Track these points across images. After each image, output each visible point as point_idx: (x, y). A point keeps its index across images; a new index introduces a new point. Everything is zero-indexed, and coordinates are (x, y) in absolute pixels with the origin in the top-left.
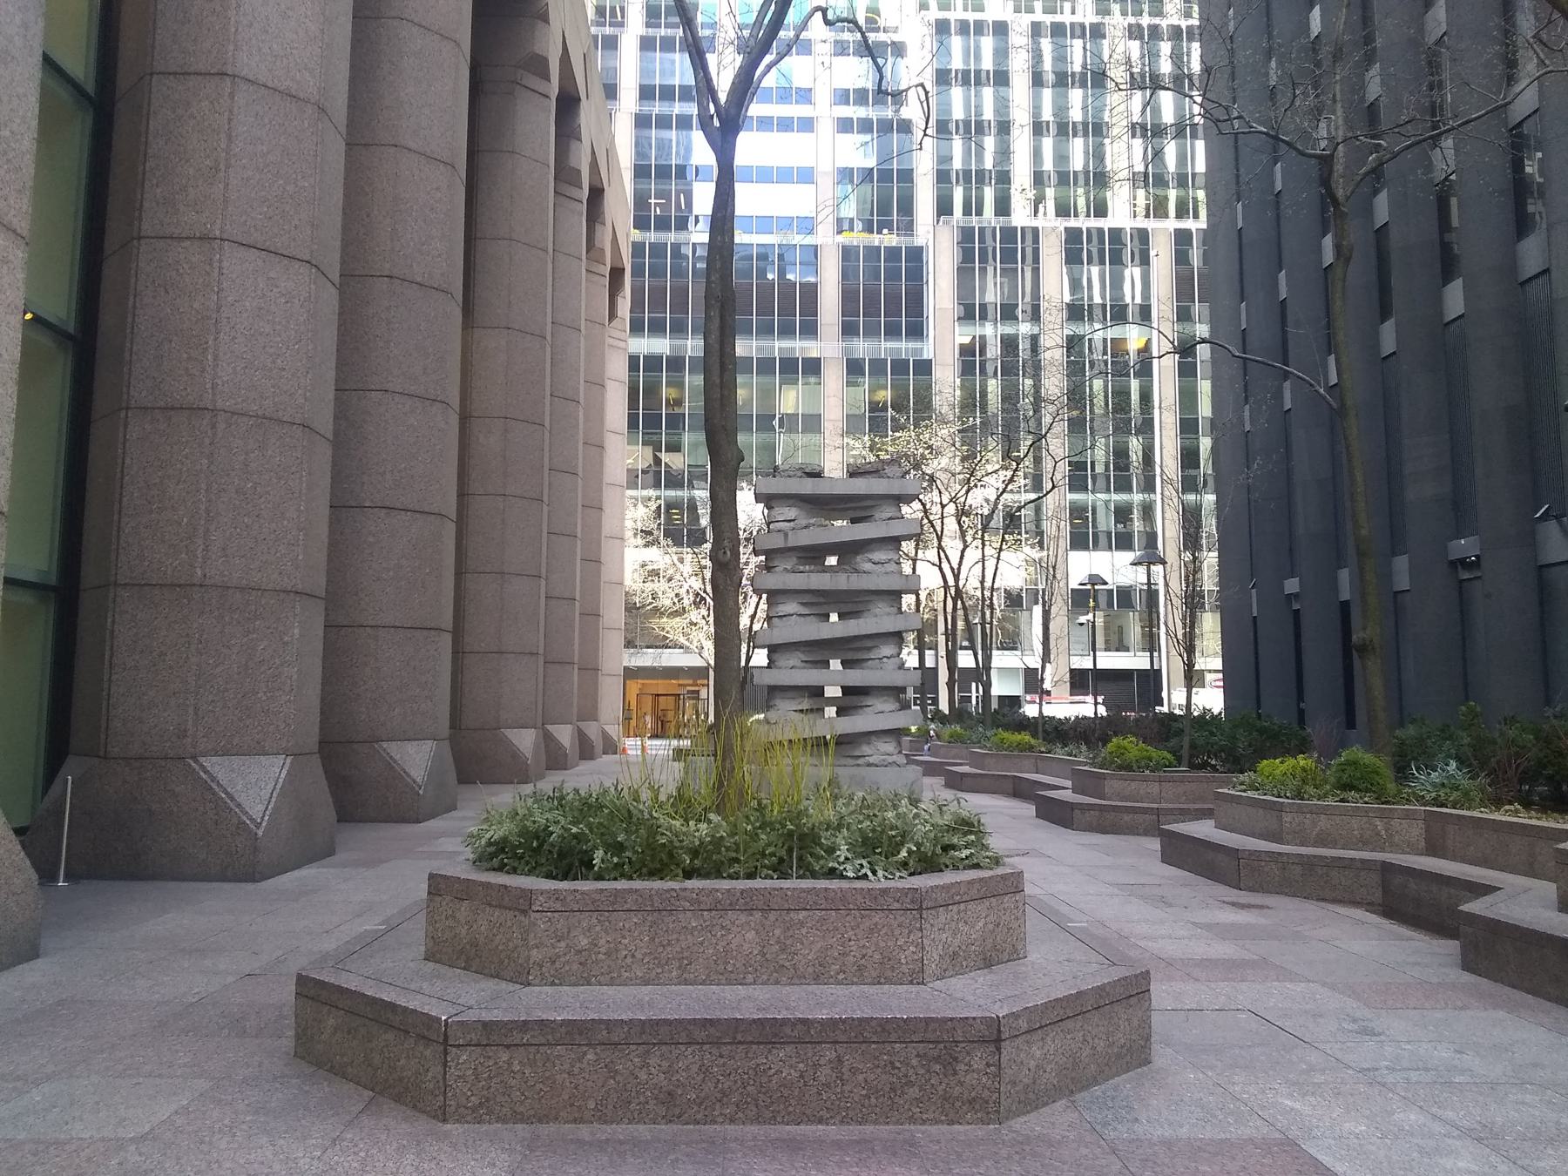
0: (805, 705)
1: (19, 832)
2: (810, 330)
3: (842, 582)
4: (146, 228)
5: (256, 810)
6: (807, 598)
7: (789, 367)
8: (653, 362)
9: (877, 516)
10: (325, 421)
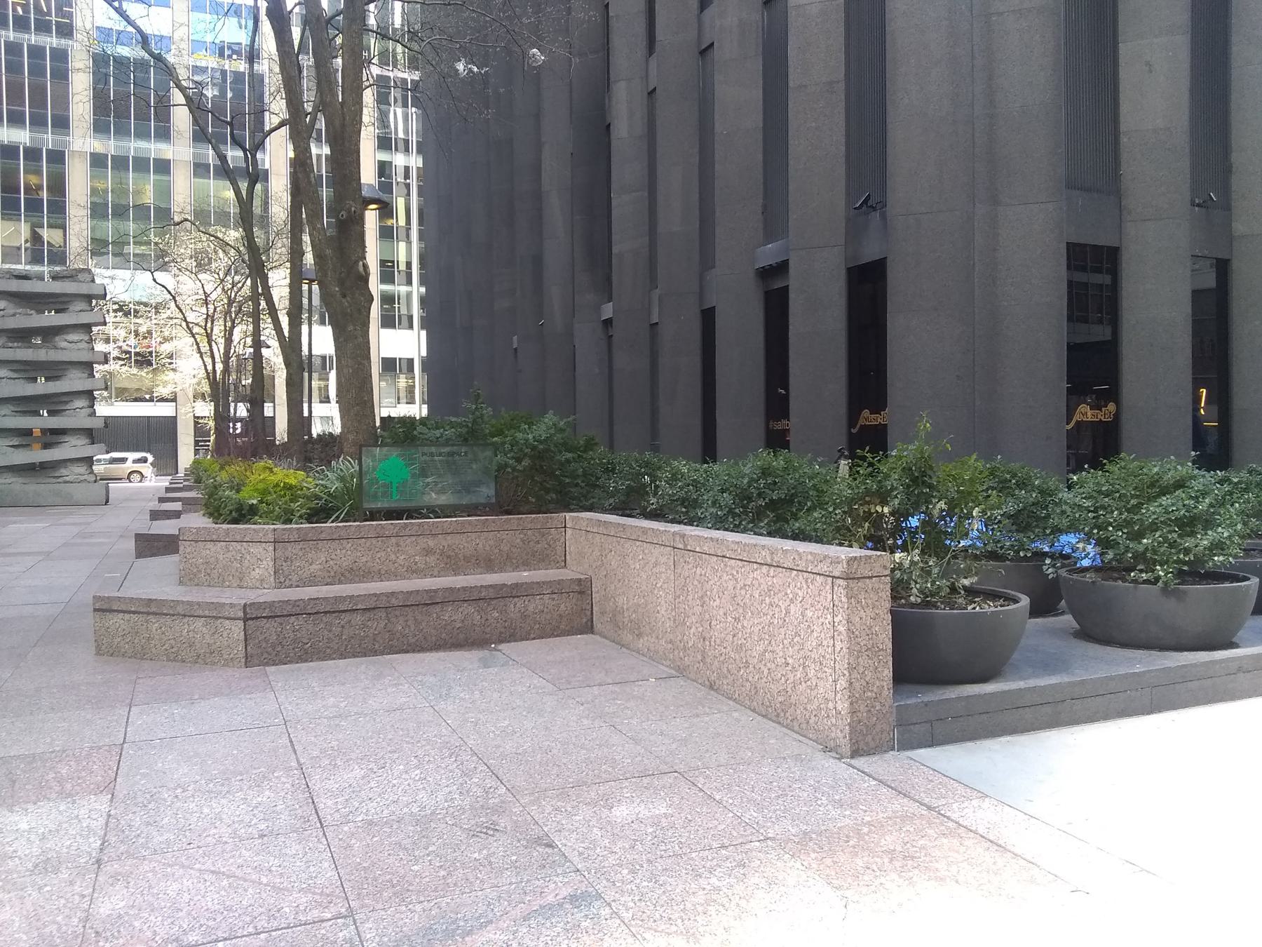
0: (16, 442)
2: (164, 134)
3: (42, 355)
6: (15, 367)
7: (142, 164)
9: (71, 308)
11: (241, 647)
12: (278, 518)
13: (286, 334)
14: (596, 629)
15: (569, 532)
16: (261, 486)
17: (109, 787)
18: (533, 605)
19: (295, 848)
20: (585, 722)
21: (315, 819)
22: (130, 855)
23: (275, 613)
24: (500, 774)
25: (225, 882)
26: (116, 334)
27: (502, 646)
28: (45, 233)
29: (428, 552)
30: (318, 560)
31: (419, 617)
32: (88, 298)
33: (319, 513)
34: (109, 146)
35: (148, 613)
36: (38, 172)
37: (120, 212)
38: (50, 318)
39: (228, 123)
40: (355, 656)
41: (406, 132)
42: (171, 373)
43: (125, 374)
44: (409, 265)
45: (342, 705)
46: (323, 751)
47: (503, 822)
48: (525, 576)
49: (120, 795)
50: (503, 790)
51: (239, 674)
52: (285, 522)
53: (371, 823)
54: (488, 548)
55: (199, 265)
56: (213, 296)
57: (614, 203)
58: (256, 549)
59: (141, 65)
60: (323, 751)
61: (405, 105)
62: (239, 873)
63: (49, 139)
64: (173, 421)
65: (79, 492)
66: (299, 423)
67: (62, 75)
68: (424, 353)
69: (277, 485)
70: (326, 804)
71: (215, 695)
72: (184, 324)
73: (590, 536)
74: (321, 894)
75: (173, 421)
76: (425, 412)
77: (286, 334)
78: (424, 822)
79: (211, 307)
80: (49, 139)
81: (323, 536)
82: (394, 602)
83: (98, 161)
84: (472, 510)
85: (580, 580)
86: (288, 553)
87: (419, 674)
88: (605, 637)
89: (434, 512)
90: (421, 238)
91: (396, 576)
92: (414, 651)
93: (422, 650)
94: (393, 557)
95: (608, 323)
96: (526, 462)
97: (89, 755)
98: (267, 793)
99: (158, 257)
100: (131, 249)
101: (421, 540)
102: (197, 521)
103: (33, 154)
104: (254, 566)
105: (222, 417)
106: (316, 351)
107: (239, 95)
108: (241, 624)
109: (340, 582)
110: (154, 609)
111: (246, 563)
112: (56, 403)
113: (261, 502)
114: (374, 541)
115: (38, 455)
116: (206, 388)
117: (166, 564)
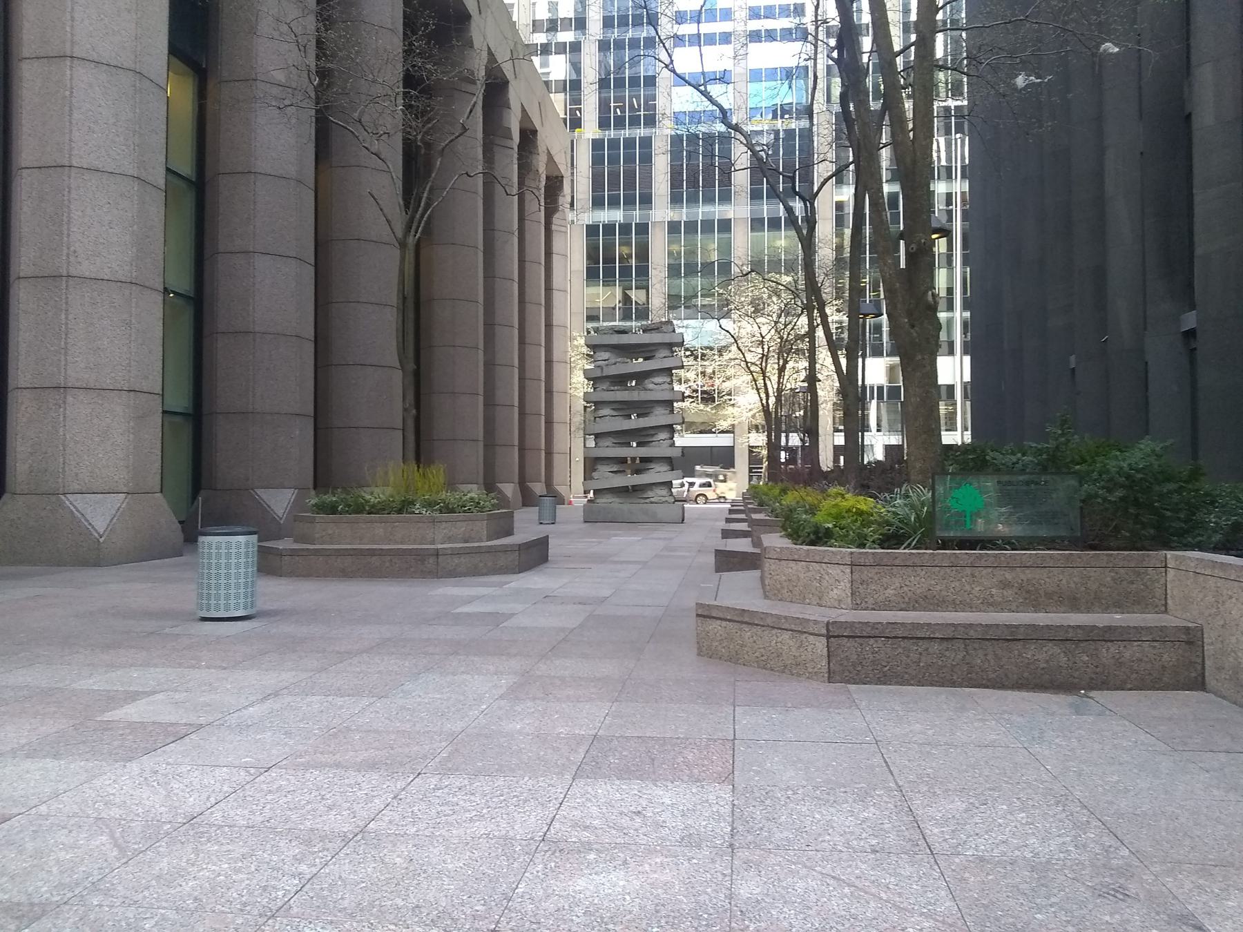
1: (180, 522)
3: (635, 396)
4: (221, 248)
5: (280, 512)
7: (708, 226)
8: (609, 228)
9: (657, 355)
10: (310, 332)
11: (824, 663)
12: (851, 543)
13: (844, 368)
14: (1208, 687)
15: (1171, 573)
16: (834, 511)
17: (728, 778)
18: (1130, 652)
19: (907, 870)
20: (1216, 792)
21: (919, 843)
22: (757, 846)
23: (859, 634)
24: (1119, 834)
25: (847, 890)
26: (690, 377)
27: (1093, 694)
28: (634, 295)
29: (1005, 585)
30: (893, 585)
31: (999, 652)
32: (670, 346)
33: (892, 539)
34: (683, 214)
35: (742, 622)
36: (629, 244)
37: (691, 270)
38: (639, 364)
39: (782, 174)
40: (932, 685)
41: (949, 159)
42: (730, 408)
43: (692, 408)
44: (950, 291)
45: (930, 732)
46: (920, 777)
47: (1133, 888)
48: (1117, 618)
49: (740, 787)
50: (1127, 853)
51: (823, 688)
52: (859, 547)
53: (982, 859)
54: (1073, 585)
55: (756, 311)
56: (767, 338)
57: (1198, 199)
58: (835, 571)
59: (725, 139)
60: (920, 777)
61: (948, 132)
62: (857, 883)
63: (637, 215)
64: (731, 450)
65: (661, 511)
66: (853, 448)
67: (647, 159)
68: (967, 377)
69: (849, 511)
70: (933, 831)
71: (807, 705)
72: (743, 364)
73: (1201, 578)
74: (943, 922)
75: (731, 450)
76: (968, 437)
77: (844, 368)
78: (1041, 869)
79: (766, 347)
80: (637, 215)
81: (897, 562)
82: (972, 633)
83: (673, 227)
84: (1050, 543)
85: (1188, 629)
86: (864, 577)
87: (1005, 712)
88: (1224, 698)
89: (1009, 543)
90: (965, 262)
91: (971, 607)
92: (994, 688)
93: (1003, 687)
94: (967, 587)
95: (1190, 334)
96: (1119, 493)
97: (707, 746)
98: (872, 809)
99: (721, 307)
100: (699, 301)
101: (998, 572)
102: (775, 541)
103: (626, 228)
104: (829, 587)
105: (774, 447)
106: (868, 382)
107: (789, 151)
108: (824, 640)
109: (914, 609)
110: (746, 619)
111: (825, 583)
112: (643, 436)
113: (835, 526)
114: (948, 570)
115: (631, 480)
116: (760, 420)
117: (748, 578)
